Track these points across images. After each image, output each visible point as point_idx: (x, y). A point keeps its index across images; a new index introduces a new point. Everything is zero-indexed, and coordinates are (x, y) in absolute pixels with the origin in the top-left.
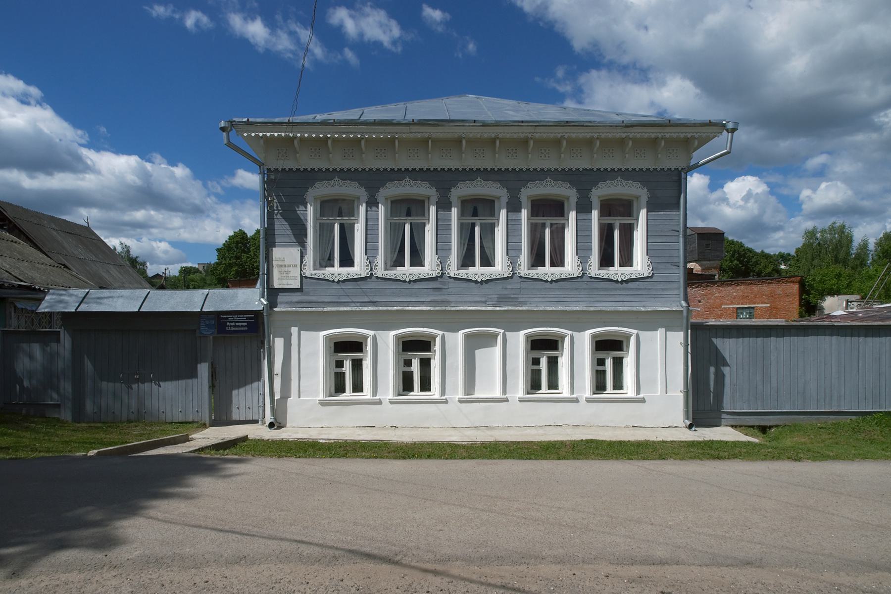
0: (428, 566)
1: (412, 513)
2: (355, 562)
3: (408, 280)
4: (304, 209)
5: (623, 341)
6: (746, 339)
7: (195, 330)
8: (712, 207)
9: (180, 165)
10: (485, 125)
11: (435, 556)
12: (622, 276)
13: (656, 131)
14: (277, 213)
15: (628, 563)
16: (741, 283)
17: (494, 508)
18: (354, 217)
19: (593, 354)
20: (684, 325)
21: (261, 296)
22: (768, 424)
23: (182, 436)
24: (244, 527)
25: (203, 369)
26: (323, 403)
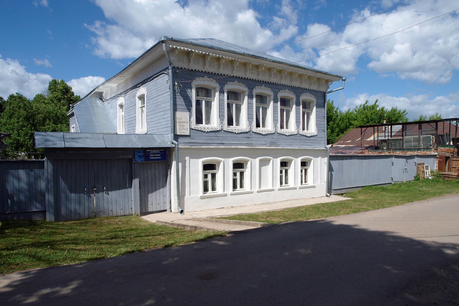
4: (190, 91)
12: (207, 129)
14: (178, 92)
18: (211, 98)
25: (136, 182)
26: (202, 198)
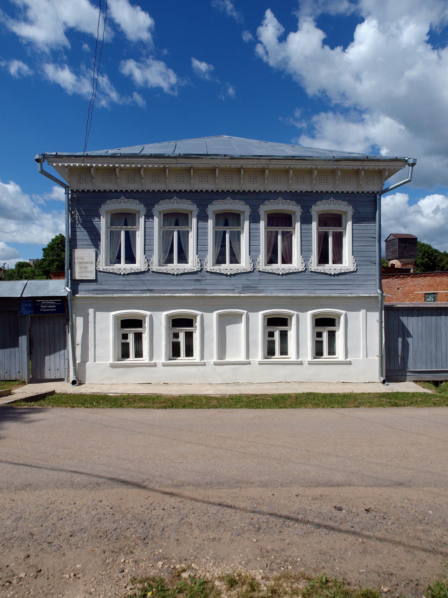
0: (168, 490)
1: (163, 450)
2: (113, 487)
3: (176, 273)
4: (99, 220)
5: (335, 319)
6: (424, 317)
7: (17, 311)
8: (410, 218)
9: (11, 182)
10: (232, 158)
11: (173, 482)
12: (334, 271)
13: (359, 164)
14: (78, 223)
15: (314, 485)
16: (428, 275)
17: (224, 445)
18: (135, 226)
19: (313, 329)
20: (380, 307)
21: (66, 285)
22: (439, 379)
23: (6, 391)
24: (34, 461)
25: (23, 340)
26: (113, 366)
